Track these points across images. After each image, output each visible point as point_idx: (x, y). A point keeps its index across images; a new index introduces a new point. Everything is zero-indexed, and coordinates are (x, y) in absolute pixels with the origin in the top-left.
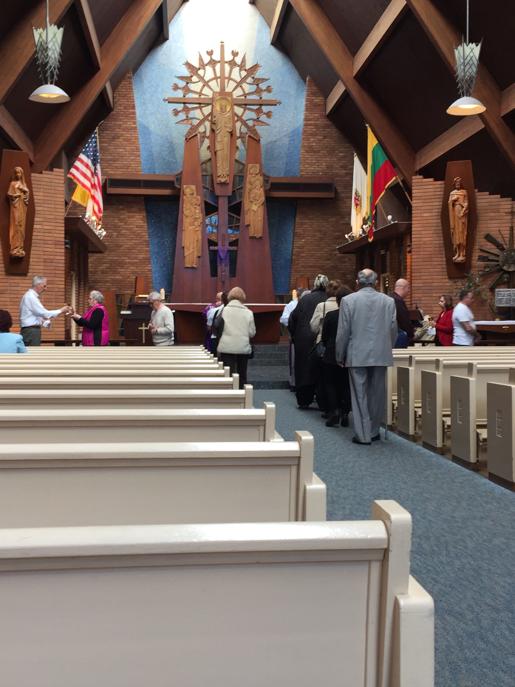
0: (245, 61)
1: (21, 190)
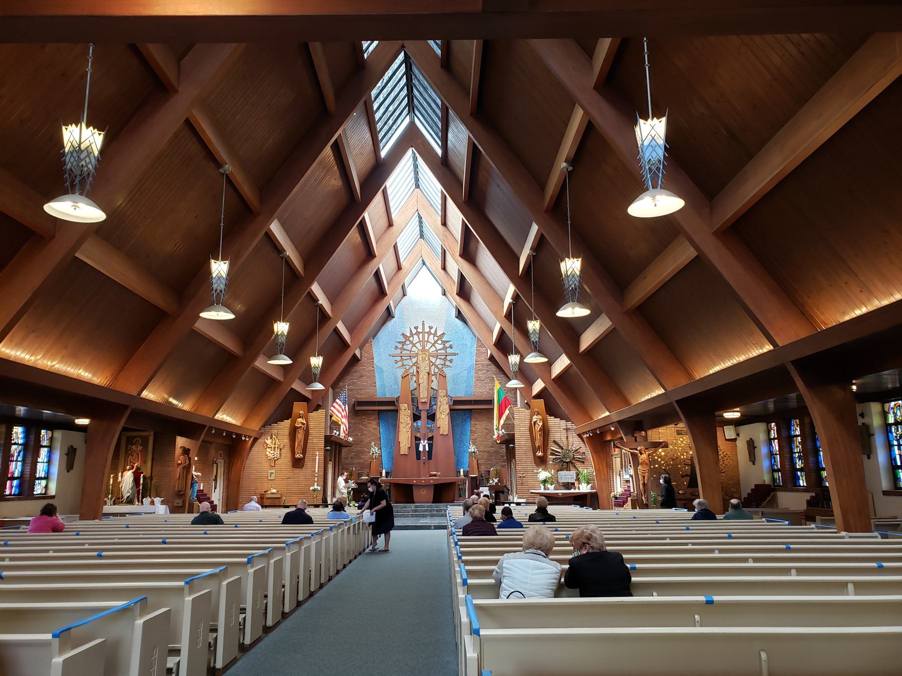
1: (302, 423)
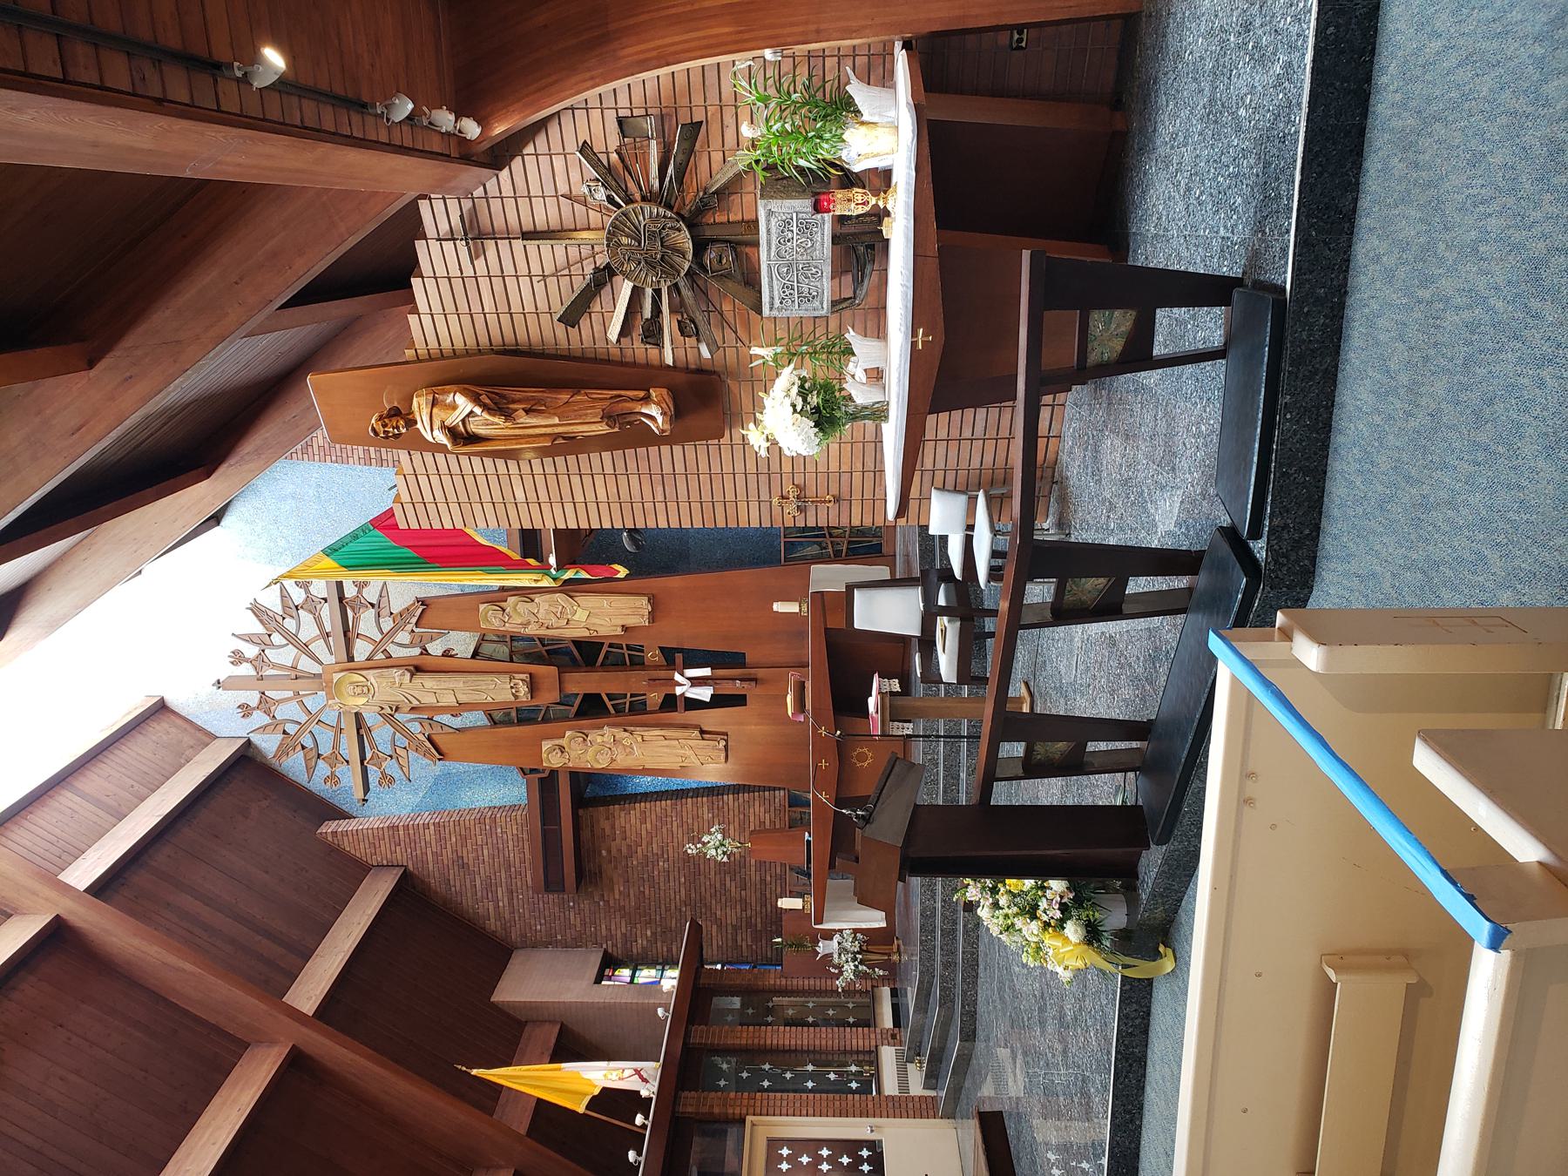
0: (248, 635)
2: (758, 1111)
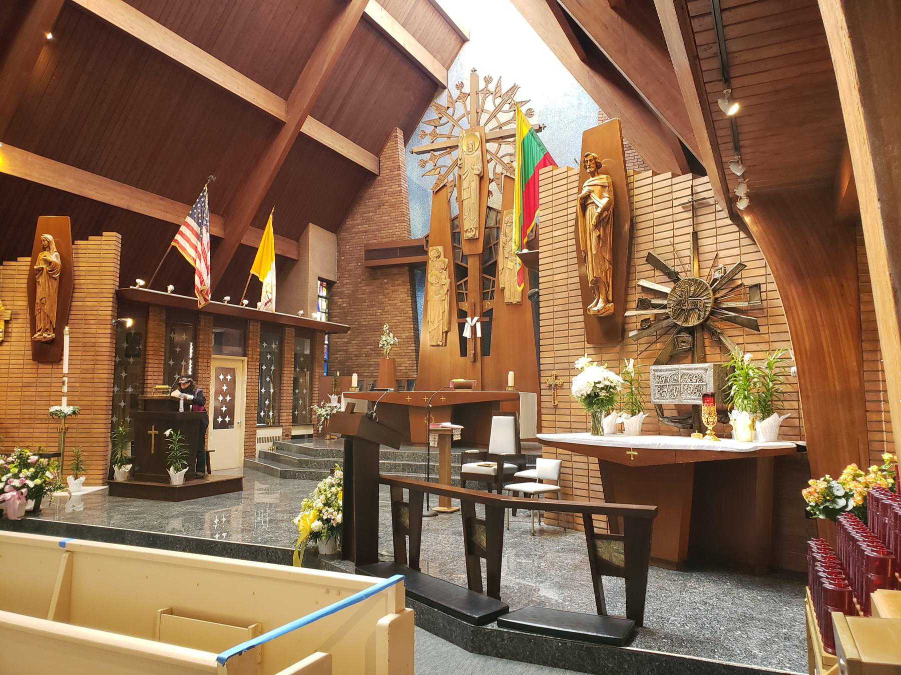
2: (250, 363)
